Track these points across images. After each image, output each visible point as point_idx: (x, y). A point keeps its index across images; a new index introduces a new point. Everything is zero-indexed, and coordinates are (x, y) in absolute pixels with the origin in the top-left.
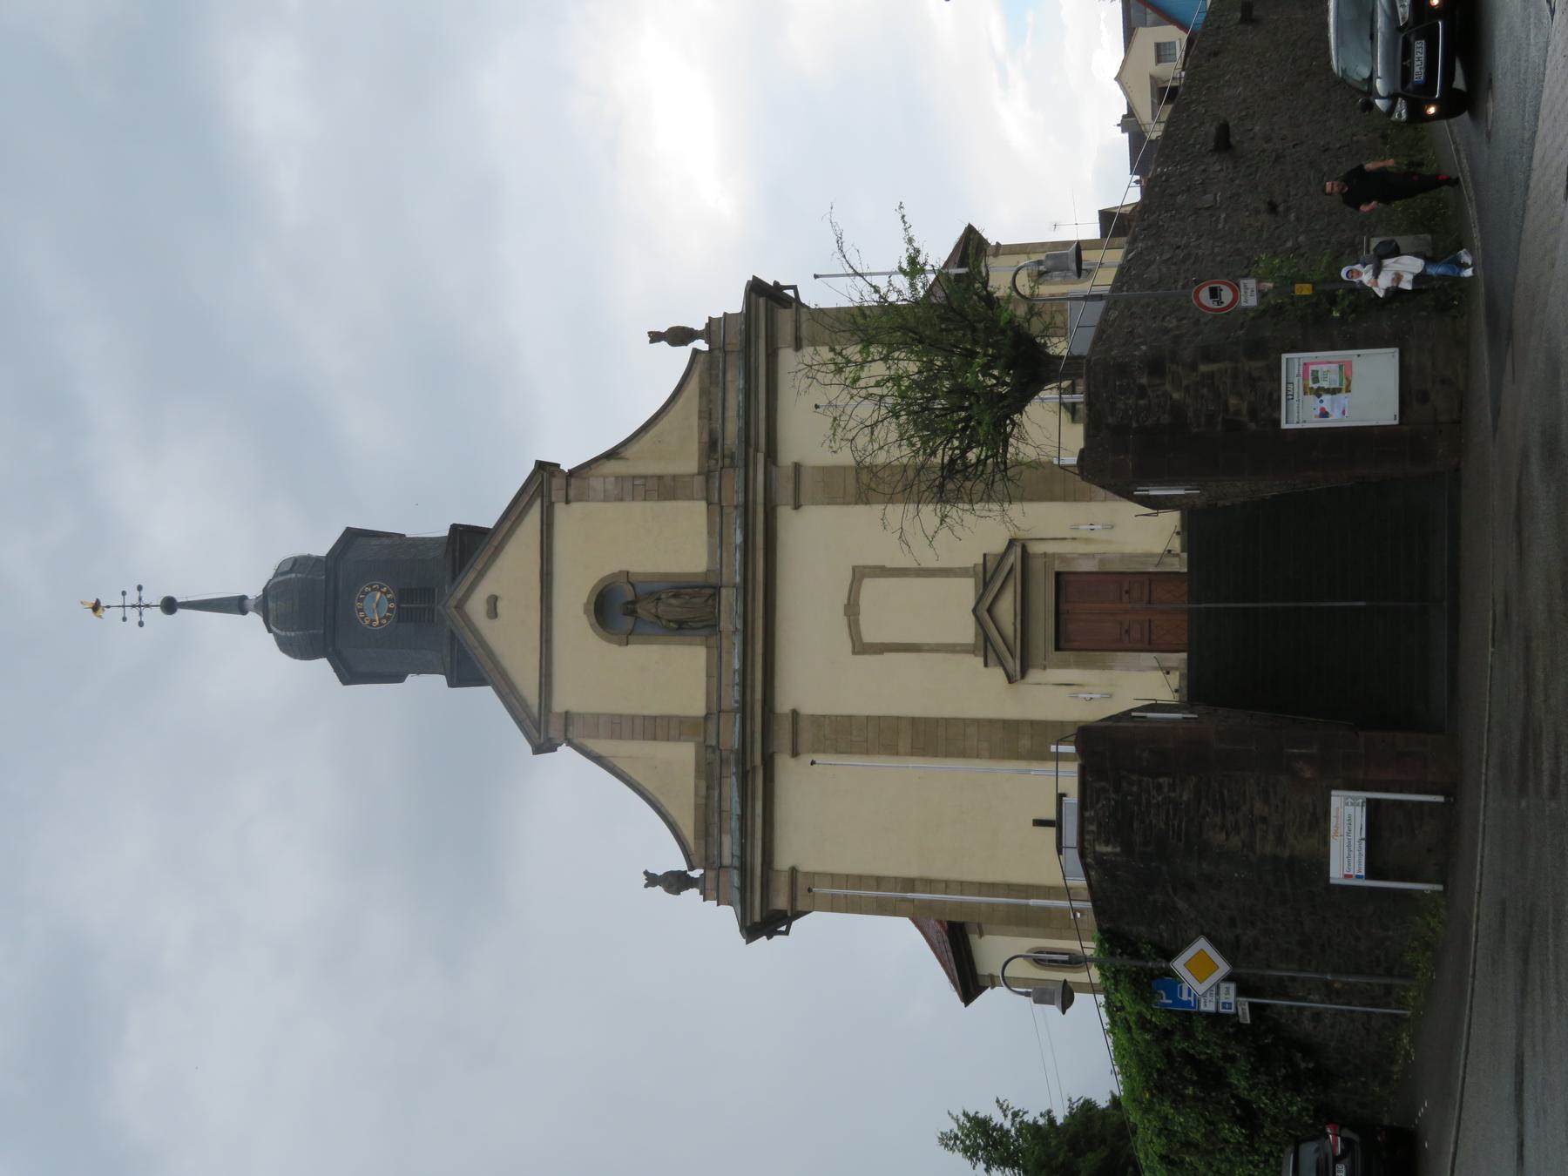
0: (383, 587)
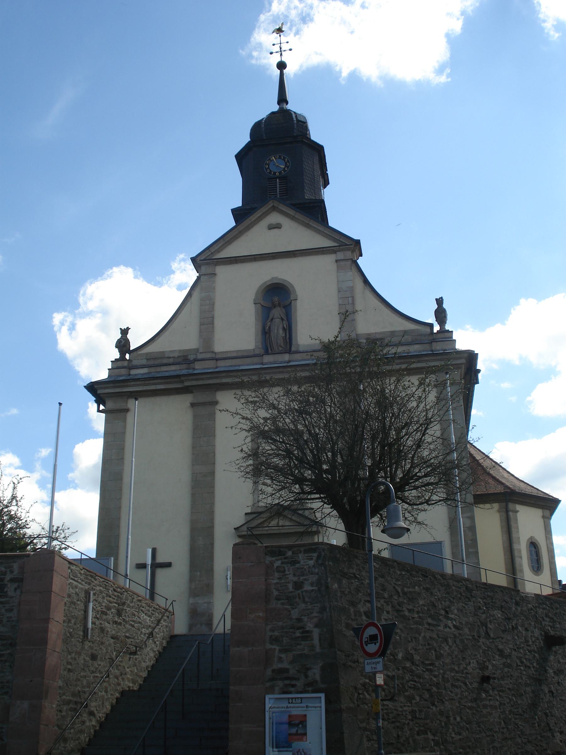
0: (288, 168)
